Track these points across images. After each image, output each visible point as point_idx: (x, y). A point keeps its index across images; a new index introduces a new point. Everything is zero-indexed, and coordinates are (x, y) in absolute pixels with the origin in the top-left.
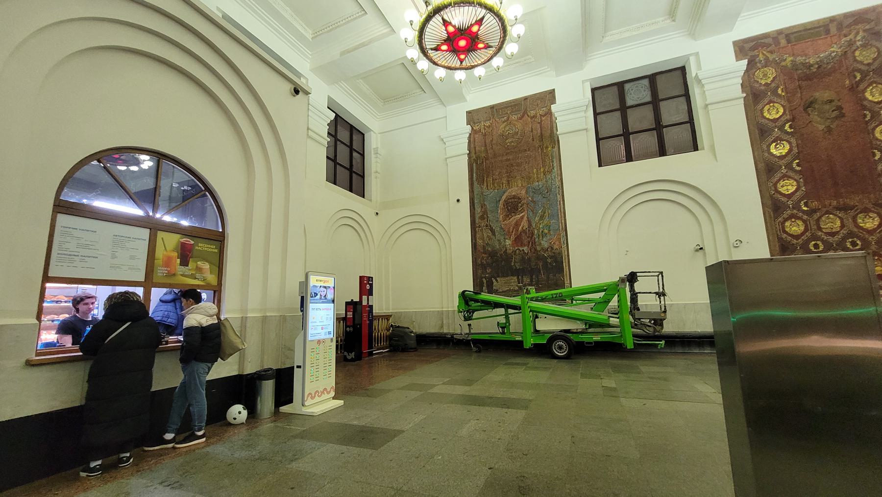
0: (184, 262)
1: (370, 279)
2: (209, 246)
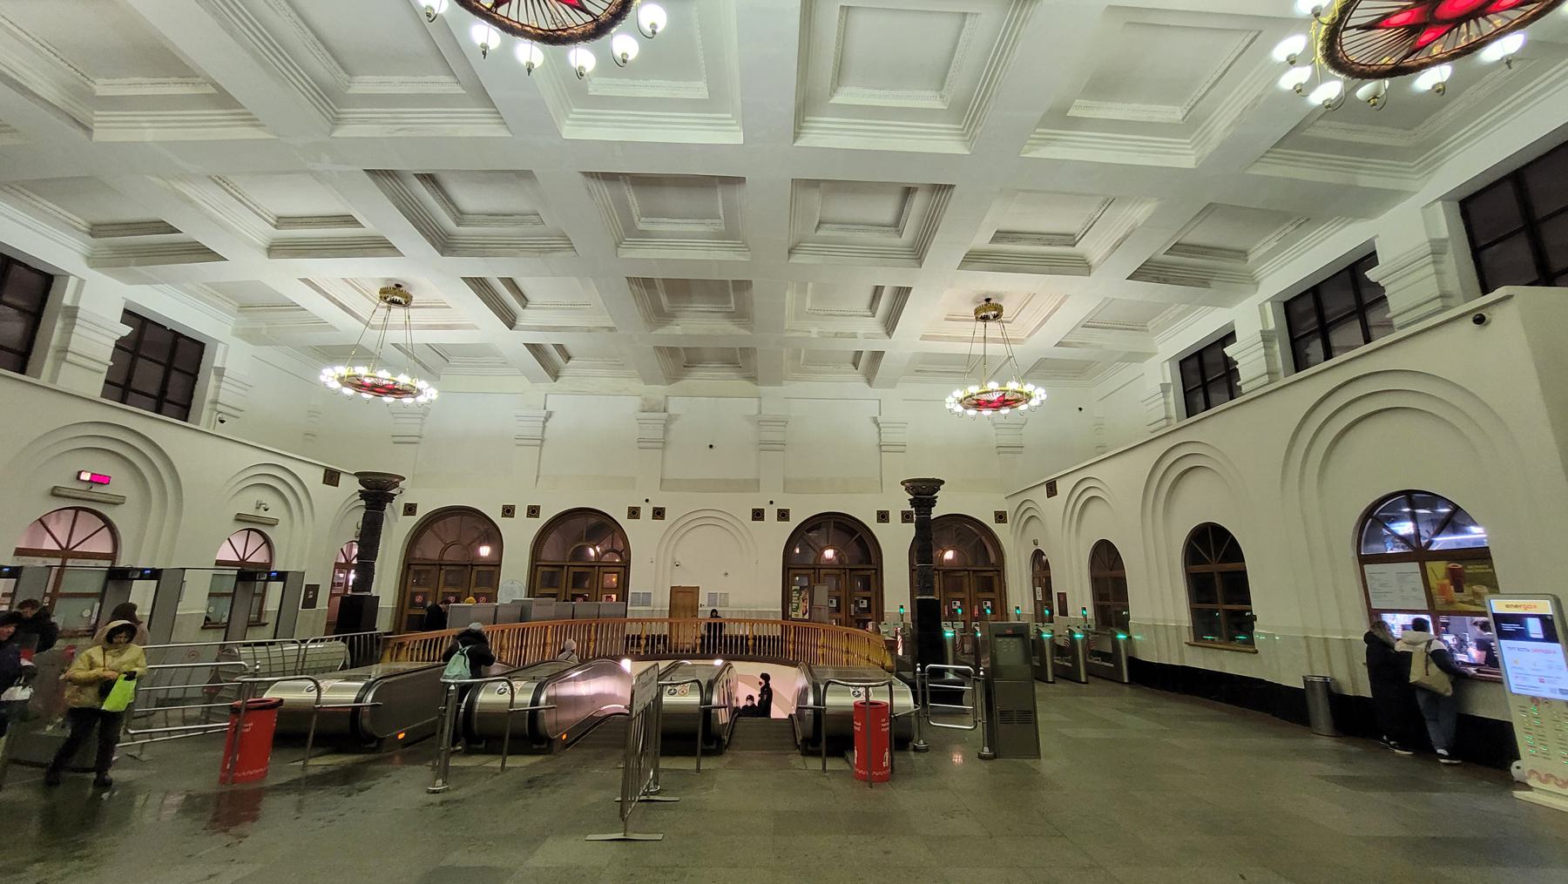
0: (1459, 589)
1: (1064, 594)
2: (1481, 566)
